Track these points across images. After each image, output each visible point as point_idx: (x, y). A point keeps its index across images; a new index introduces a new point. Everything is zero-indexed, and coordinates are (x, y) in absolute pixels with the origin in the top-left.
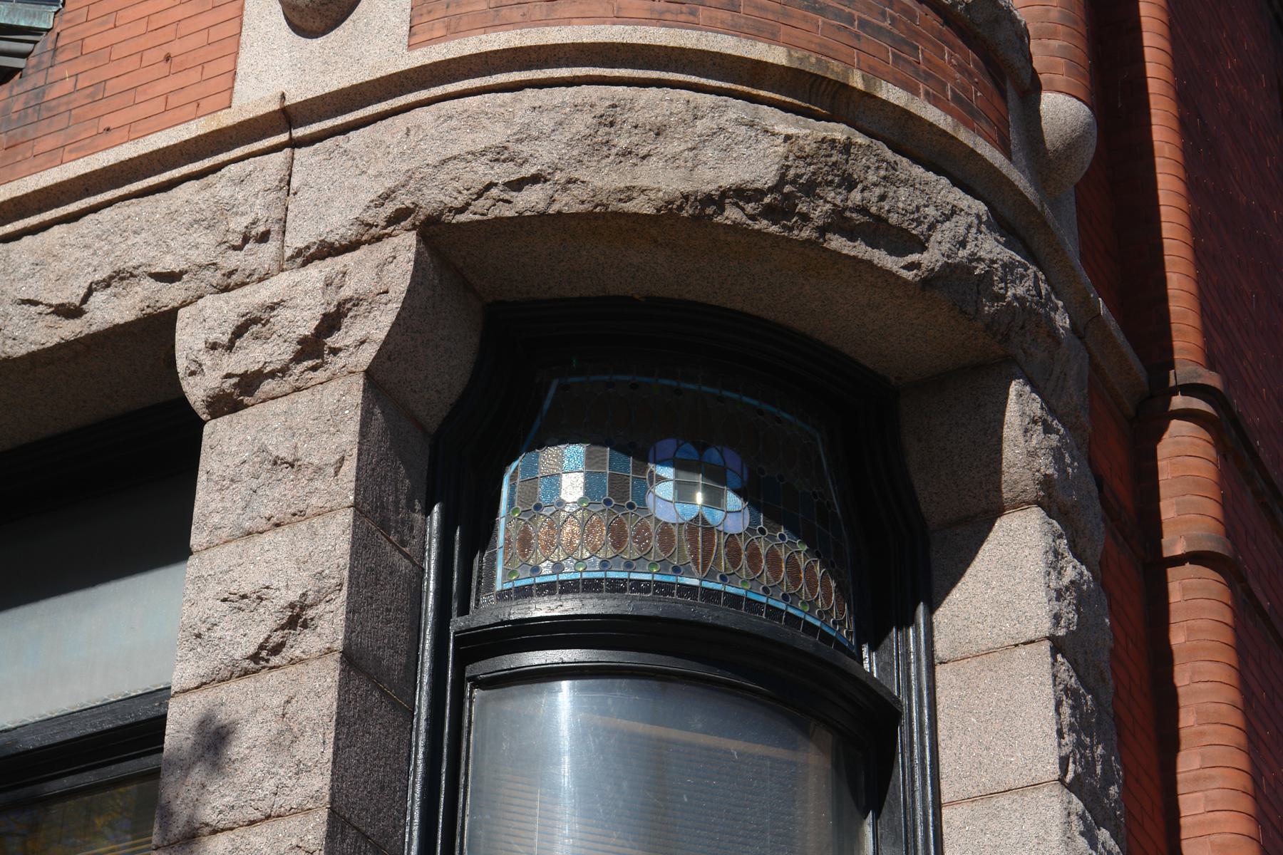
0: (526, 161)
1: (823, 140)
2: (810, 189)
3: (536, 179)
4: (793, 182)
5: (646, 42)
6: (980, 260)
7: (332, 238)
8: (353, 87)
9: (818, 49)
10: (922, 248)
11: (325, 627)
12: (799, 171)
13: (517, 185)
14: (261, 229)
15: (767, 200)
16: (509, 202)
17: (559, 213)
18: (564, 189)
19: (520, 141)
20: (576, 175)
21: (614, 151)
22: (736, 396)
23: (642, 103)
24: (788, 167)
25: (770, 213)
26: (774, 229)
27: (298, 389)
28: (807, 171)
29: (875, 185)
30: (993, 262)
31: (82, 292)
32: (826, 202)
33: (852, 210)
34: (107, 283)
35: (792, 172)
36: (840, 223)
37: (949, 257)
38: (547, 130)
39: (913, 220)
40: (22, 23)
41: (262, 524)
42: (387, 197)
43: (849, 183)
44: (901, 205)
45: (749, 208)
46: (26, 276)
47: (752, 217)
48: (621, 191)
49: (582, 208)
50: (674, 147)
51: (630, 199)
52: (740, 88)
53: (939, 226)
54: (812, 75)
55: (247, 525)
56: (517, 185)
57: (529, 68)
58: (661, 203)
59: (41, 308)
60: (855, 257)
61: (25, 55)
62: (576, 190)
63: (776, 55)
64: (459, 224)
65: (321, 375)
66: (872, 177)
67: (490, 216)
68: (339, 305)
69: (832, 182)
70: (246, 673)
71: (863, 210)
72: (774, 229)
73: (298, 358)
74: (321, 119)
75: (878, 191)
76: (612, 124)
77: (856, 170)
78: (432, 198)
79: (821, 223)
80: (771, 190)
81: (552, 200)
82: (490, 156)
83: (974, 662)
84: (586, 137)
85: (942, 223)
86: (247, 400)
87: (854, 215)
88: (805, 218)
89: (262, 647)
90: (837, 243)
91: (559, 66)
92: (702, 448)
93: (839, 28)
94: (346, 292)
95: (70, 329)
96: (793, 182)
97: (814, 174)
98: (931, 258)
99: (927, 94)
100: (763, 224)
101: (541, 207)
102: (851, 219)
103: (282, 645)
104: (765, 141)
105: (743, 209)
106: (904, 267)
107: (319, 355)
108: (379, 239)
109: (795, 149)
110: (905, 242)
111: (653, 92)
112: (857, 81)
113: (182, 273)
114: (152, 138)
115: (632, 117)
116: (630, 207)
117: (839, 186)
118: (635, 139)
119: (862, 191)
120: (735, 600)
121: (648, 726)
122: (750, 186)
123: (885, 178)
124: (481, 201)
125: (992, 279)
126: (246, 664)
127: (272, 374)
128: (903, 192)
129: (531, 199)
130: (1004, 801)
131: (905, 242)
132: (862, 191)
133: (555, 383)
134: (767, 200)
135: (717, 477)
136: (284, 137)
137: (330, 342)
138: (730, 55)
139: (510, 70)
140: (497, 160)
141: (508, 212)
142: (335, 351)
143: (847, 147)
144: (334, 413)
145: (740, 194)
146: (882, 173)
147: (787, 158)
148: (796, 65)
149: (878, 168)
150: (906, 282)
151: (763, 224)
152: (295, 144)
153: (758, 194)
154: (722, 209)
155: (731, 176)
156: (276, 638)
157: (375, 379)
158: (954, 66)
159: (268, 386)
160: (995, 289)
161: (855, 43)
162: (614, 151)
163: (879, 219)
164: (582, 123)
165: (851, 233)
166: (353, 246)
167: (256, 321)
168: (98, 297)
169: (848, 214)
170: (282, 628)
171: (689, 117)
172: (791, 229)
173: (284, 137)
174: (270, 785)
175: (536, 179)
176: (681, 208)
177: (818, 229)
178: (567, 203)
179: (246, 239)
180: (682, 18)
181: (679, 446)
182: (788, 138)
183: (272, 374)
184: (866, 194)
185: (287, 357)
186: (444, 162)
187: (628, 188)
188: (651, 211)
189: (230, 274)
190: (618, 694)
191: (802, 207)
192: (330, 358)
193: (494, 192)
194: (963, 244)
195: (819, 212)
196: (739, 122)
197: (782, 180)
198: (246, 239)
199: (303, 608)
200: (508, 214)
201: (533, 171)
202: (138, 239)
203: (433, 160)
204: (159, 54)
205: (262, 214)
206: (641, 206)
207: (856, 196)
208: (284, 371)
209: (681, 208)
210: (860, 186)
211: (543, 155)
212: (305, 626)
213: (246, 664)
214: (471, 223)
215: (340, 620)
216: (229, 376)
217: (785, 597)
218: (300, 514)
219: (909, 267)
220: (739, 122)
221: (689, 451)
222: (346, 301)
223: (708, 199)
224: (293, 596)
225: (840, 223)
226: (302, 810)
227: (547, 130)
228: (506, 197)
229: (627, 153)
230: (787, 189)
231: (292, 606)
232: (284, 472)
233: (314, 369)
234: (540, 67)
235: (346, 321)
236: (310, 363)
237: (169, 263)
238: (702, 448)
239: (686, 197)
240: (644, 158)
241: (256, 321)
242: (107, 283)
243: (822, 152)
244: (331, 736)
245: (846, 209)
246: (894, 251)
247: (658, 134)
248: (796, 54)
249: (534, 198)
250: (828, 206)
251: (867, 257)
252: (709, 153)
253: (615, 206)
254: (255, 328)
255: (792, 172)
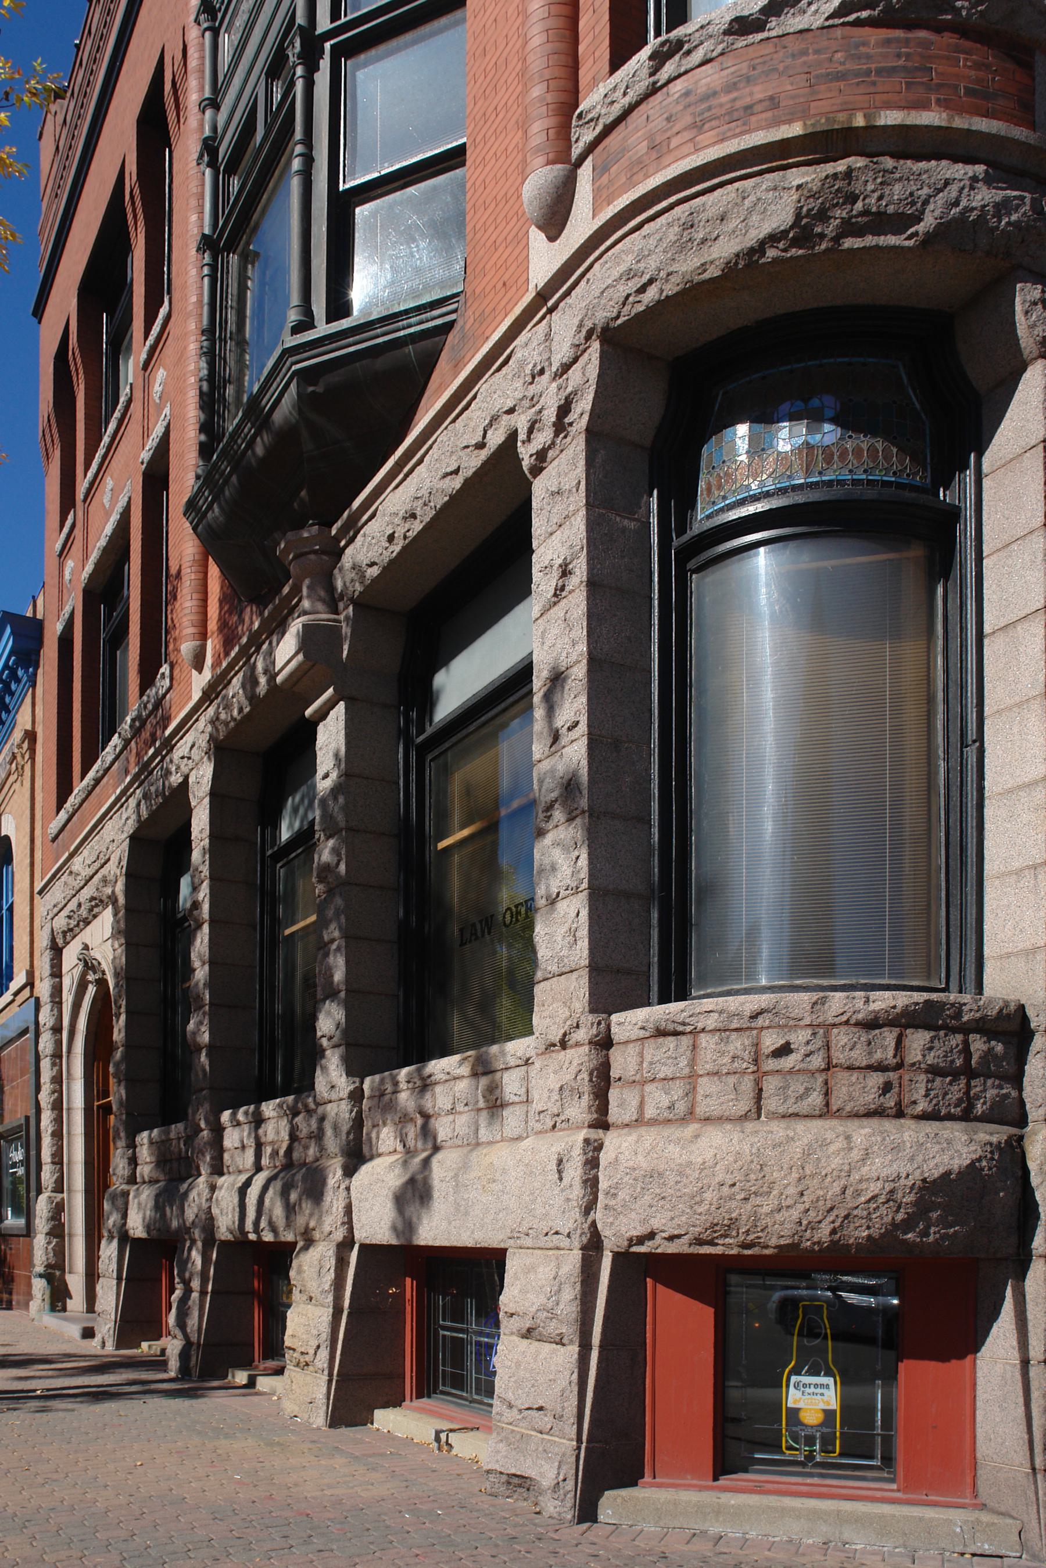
0: (643, 273)
1: (827, 177)
2: (822, 215)
3: (651, 281)
4: (807, 216)
5: (705, 161)
6: (973, 209)
7: (564, 360)
8: (563, 265)
9: (840, 108)
10: (919, 220)
11: (577, 571)
12: (810, 206)
13: (642, 290)
14: (539, 368)
15: (791, 235)
16: (639, 302)
17: (667, 297)
18: (667, 281)
19: (639, 261)
20: (671, 269)
21: (695, 243)
22: (832, 360)
23: (710, 203)
24: (801, 207)
25: (795, 243)
26: (801, 252)
27: (562, 451)
28: (815, 204)
29: (873, 191)
30: (983, 206)
31: (482, 433)
32: (836, 218)
33: (856, 216)
34: (490, 424)
35: (805, 209)
36: (849, 229)
37: (941, 218)
38: (652, 247)
39: (907, 204)
40: (449, 294)
41: (555, 527)
42: (580, 326)
43: (852, 198)
44: (896, 197)
45: (781, 245)
46: (463, 434)
47: (785, 250)
48: (699, 268)
49: (678, 289)
50: (733, 224)
51: (705, 271)
52: (774, 164)
53: (932, 200)
54: (823, 132)
55: (549, 530)
56: (642, 290)
57: (644, 211)
58: (723, 266)
59: (471, 448)
60: (864, 247)
61: (455, 311)
62: (673, 279)
63: (795, 130)
64: (619, 326)
65: (569, 439)
66: (870, 187)
67: (633, 314)
68: (566, 398)
69: (838, 203)
70: (555, 604)
71: (865, 212)
72: (801, 252)
73: (556, 435)
74: (557, 291)
75: (876, 195)
76: (692, 226)
77: (857, 187)
78: (601, 317)
79: (834, 234)
80: (792, 227)
81: (662, 291)
82: (624, 278)
83: (1003, 470)
84: (675, 242)
85: (935, 196)
86: (544, 465)
87: (859, 219)
88: (822, 236)
89: (556, 590)
90: (849, 243)
91: (660, 201)
92: (806, 400)
93: (858, 84)
94: (569, 389)
95: (484, 454)
96: (807, 216)
97: (822, 203)
98: (928, 223)
99: (938, 102)
100: (793, 252)
101: (656, 297)
102: (857, 222)
103: (564, 586)
104: (785, 195)
105: (777, 248)
106: (906, 239)
107: (565, 429)
108: (585, 351)
109: (805, 192)
110: (900, 222)
111: (719, 192)
112: (860, 121)
113: (515, 406)
114: (493, 336)
115: (704, 217)
116: (707, 276)
117: (844, 204)
118: (707, 230)
119: (864, 199)
120: (830, 483)
121: (287, 636)
122: (777, 231)
123: (881, 184)
124: (626, 307)
125: (985, 218)
126: (553, 599)
127: (550, 448)
128: (897, 187)
129: (652, 295)
130: (1015, 546)
131: (900, 222)
132: (864, 199)
133: (721, 393)
134: (791, 235)
135: (815, 418)
136: (544, 310)
137: (567, 420)
138: (762, 145)
139: (634, 217)
140: (629, 279)
141: (640, 308)
142: (571, 424)
143: (849, 174)
144: (573, 459)
145: (773, 238)
146: (879, 180)
147: (799, 201)
148: (810, 130)
149: (875, 179)
150: (909, 248)
151: (793, 252)
152: (550, 311)
153: (785, 233)
154: (763, 254)
155: (767, 228)
156: (560, 584)
157: (591, 432)
158: (970, 67)
159: (551, 454)
160: (990, 224)
161: (872, 90)
162: (695, 243)
163: (879, 214)
164: (674, 232)
165: (859, 232)
166: (575, 360)
167: (535, 422)
168: (490, 433)
169: (854, 220)
170: (561, 578)
171: (739, 201)
172: (813, 248)
173: (544, 310)
174: (564, 654)
175: (651, 281)
176: (736, 263)
177: (832, 239)
178: (671, 289)
179: (533, 377)
180: (738, 131)
181: (792, 404)
182: (799, 187)
183: (550, 448)
184: (867, 201)
185: (552, 436)
186: (602, 293)
187: (702, 265)
188: (719, 273)
189: (532, 399)
190: (787, 553)
191: (818, 230)
192: (569, 429)
193: (631, 299)
194: (956, 203)
195: (830, 229)
196: (768, 190)
197: (798, 216)
198: (533, 377)
199: (566, 565)
200: (641, 309)
201: (648, 277)
202: (496, 396)
203: (597, 294)
204: (500, 284)
205: (538, 359)
206: (713, 272)
207: (859, 206)
208: (553, 443)
209: (736, 263)
210: (862, 197)
211: (651, 265)
212: (570, 573)
213: (553, 599)
214: (625, 322)
215: (584, 567)
216: (531, 456)
217: (865, 471)
218: (567, 517)
219: (909, 238)
220: (768, 190)
221: (799, 405)
222: (570, 394)
223: (752, 251)
224: (560, 561)
225: (849, 229)
226: (578, 662)
227: (652, 247)
228: (638, 299)
229: (704, 241)
230: (804, 221)
231: (561, 566)
232: (558, 498)
233: (565, 437)
234: (650, 207)
235: (573, 406)
236: (562, 436)
237: (510, 404)
238: (806, 400)
239: (737, 255)
240: (715, 239)
241: (535, 422)
242: (490, 424)
243: (827, 186)
244: (585, 624)
245: (851, 217)
246: (897, 232)
247: (722, 220)
248: (809, 123)
249: (652, 293)
250: (838, 221)
251: (874, 243)
252: (755, 218)
253: (697, 279)
254: (537, 426)
255: (805, 209)
